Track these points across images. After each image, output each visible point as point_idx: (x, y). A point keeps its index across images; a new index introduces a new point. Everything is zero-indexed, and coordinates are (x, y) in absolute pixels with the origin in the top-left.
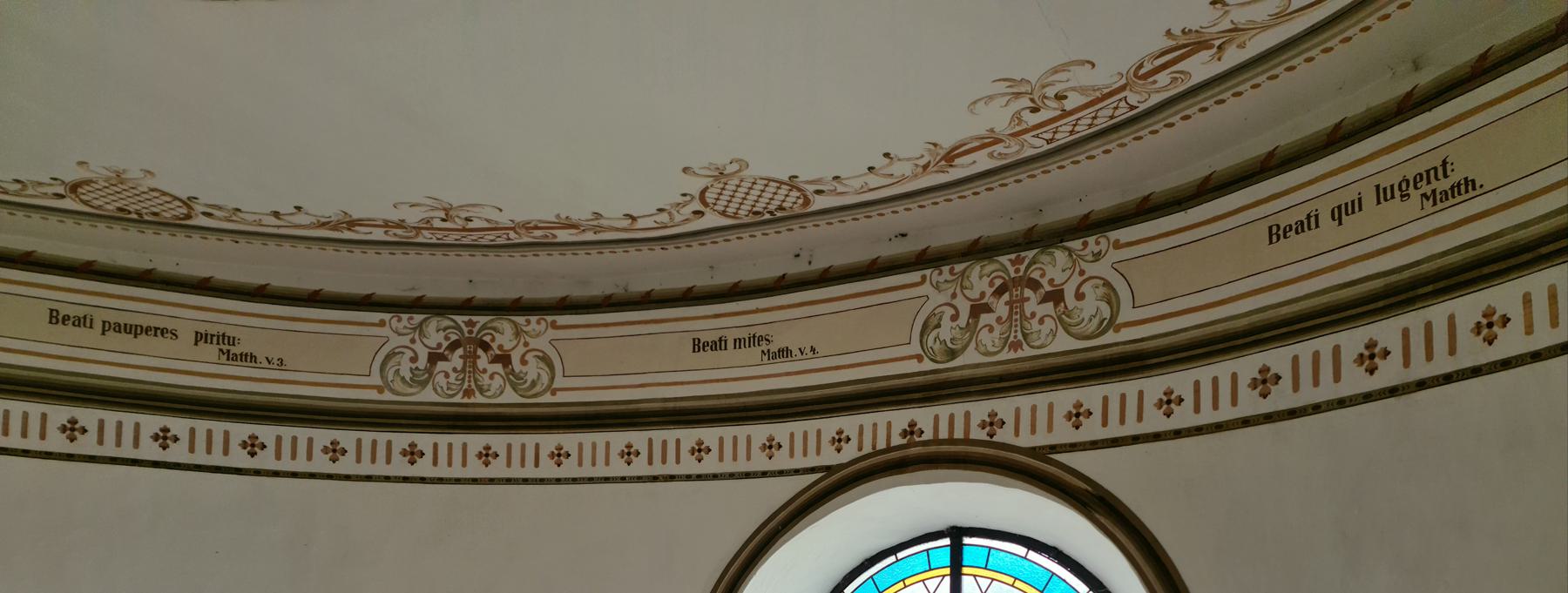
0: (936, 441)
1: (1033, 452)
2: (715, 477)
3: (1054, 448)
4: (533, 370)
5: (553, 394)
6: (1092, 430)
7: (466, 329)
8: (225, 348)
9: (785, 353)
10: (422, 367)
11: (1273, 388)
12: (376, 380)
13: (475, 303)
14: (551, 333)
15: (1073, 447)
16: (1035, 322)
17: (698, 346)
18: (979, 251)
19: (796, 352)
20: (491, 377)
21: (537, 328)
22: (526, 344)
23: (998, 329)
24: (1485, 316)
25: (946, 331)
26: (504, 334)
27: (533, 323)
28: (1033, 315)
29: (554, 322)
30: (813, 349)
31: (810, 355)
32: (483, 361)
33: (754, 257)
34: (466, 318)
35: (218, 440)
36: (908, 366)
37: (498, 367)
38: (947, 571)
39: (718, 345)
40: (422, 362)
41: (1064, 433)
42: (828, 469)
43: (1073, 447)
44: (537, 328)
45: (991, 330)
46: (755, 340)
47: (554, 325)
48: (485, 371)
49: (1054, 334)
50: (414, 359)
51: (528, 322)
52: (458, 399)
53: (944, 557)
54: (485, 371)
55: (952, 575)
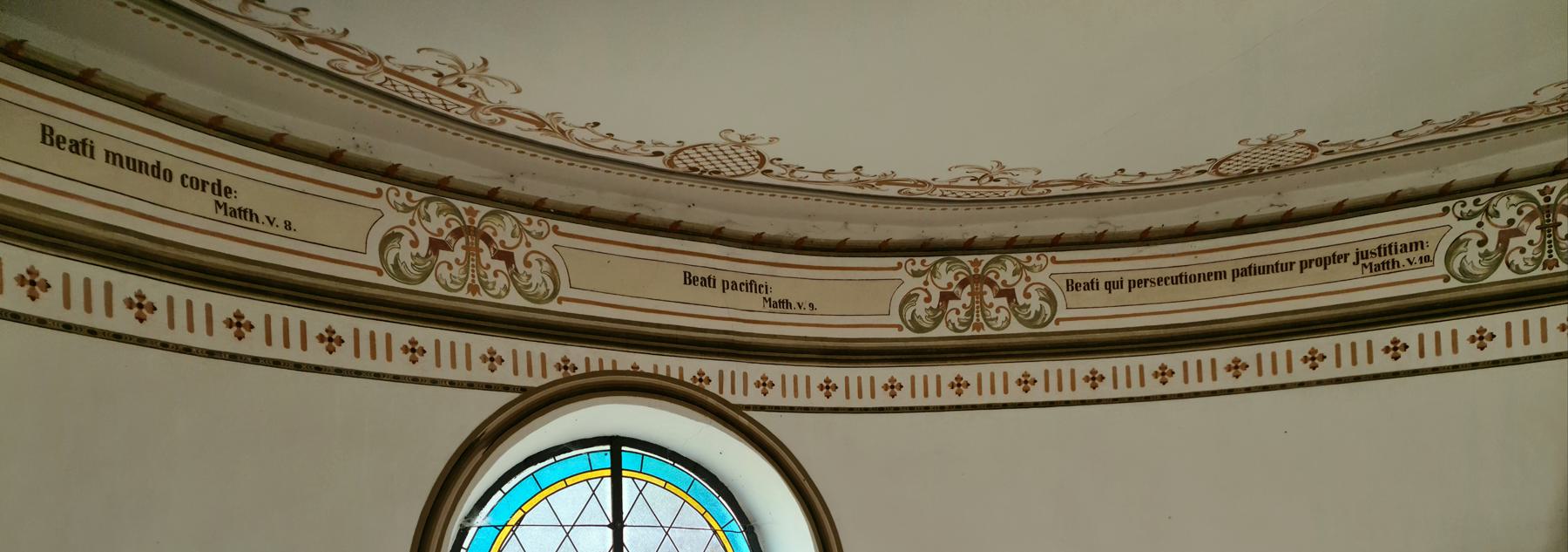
0: (589, 374)
1: (739, 408)
2: (256, 360)
3: (748, 407)
4: (537, 277)
5: (560, 302)
6: (774, 398)
7: (466, 218)
8: (222, 199)
9: (784, 304)
10: (423, 254)
11: (247, 334)
12: (373, 259)
13: (1246, 222)
14: (1052, 268)
15: (762, 408)
16: (993, 310)
17: (689, 279)
18: (441, 188)
19: (794, 305)
20: (998, 311)
21: (1038, 263)
22: (1028, 279)
23: (1530, 250)
24: (29, 272)
25: (921, 308)
26: (504, 229)
27: (536, 224)
28: (488, 266)
29: (555, 228)
30: (811, 305)
31: (808, 310)
32: (989, 297)
33: (1259, 199)
34: (467, 205)
35: (1206, 368)
36: (891, 332)
37: (1003, 301)
38: (608, 472)
39: (708, 282)
40: (423, 249)
41: (755, 397)
42: (523, 389)
43: (762, 408)
44: (1038, 263)
45: (1523, 251)
46: (751, 286)
47: (1054, 260)
48: (991, 305)
49: (1008, 321)
50: (415, 244)
51: (530, 222)
52: (463, 294)
53: (607, 460)
54: (991, 305)
55: (612, 476)
